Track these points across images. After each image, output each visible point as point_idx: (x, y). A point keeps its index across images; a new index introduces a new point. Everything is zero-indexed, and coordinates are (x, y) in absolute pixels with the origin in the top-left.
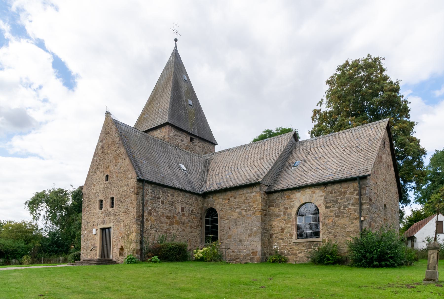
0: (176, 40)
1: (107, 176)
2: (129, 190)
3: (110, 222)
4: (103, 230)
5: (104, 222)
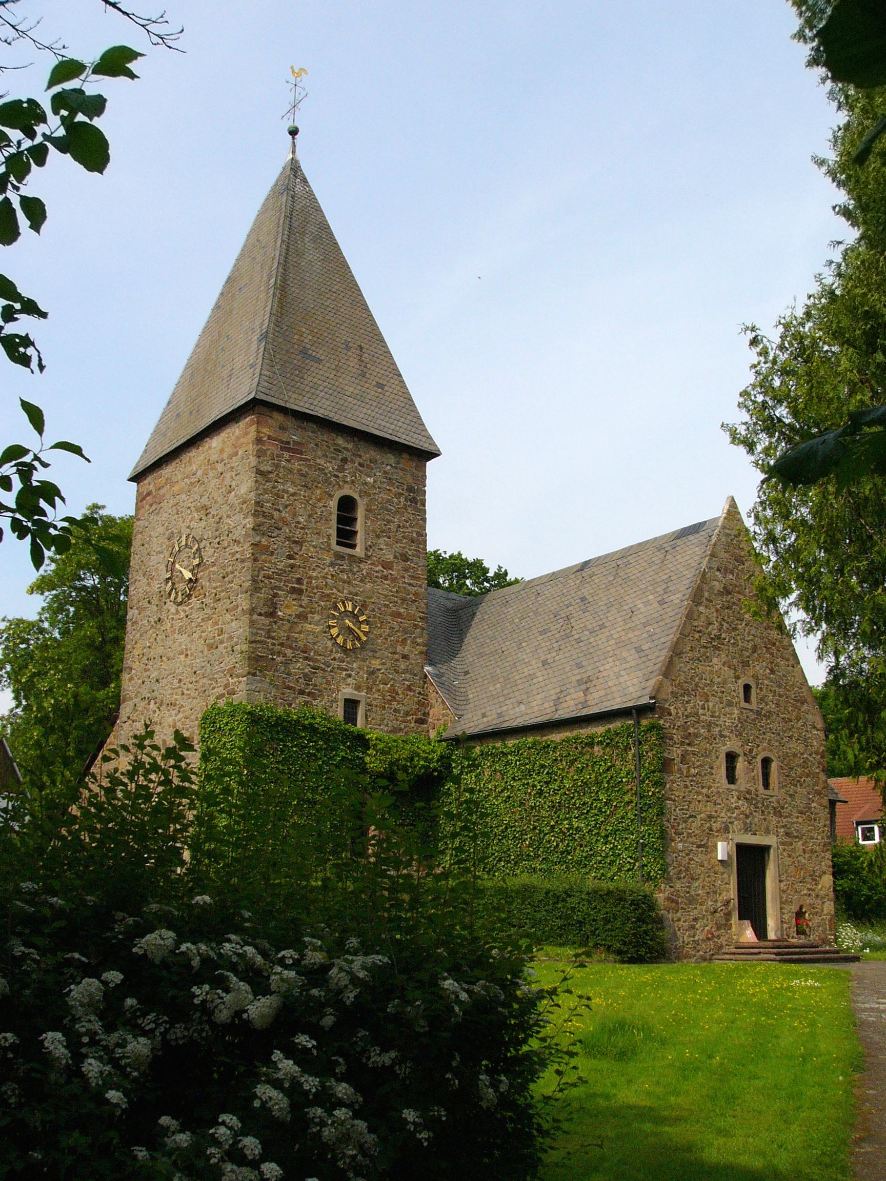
0: (294, 132)
1: (747, 688)
2: (810, 755)
3: (767, 832)
4: (743, 850)
5: (747, 829)
